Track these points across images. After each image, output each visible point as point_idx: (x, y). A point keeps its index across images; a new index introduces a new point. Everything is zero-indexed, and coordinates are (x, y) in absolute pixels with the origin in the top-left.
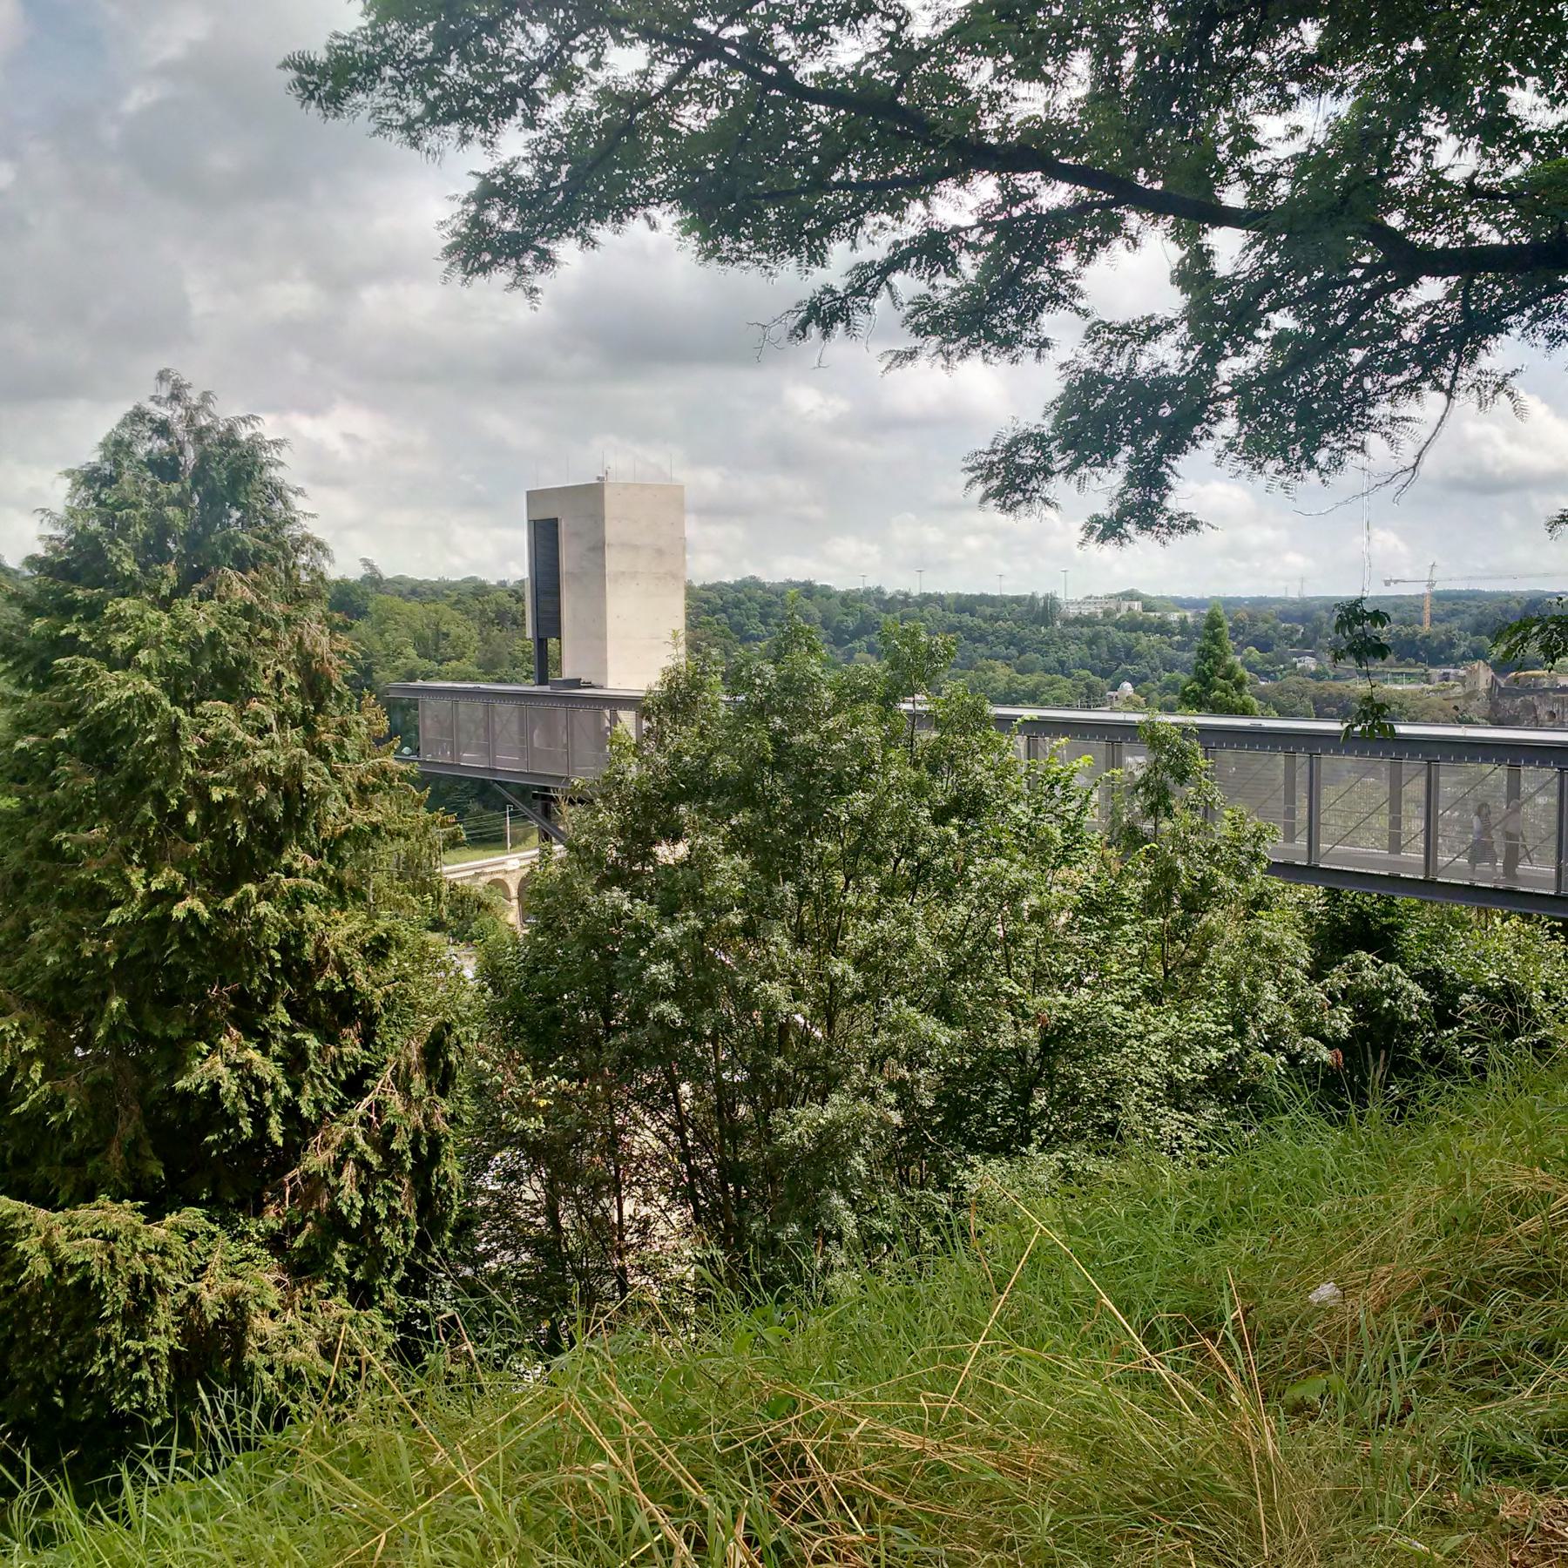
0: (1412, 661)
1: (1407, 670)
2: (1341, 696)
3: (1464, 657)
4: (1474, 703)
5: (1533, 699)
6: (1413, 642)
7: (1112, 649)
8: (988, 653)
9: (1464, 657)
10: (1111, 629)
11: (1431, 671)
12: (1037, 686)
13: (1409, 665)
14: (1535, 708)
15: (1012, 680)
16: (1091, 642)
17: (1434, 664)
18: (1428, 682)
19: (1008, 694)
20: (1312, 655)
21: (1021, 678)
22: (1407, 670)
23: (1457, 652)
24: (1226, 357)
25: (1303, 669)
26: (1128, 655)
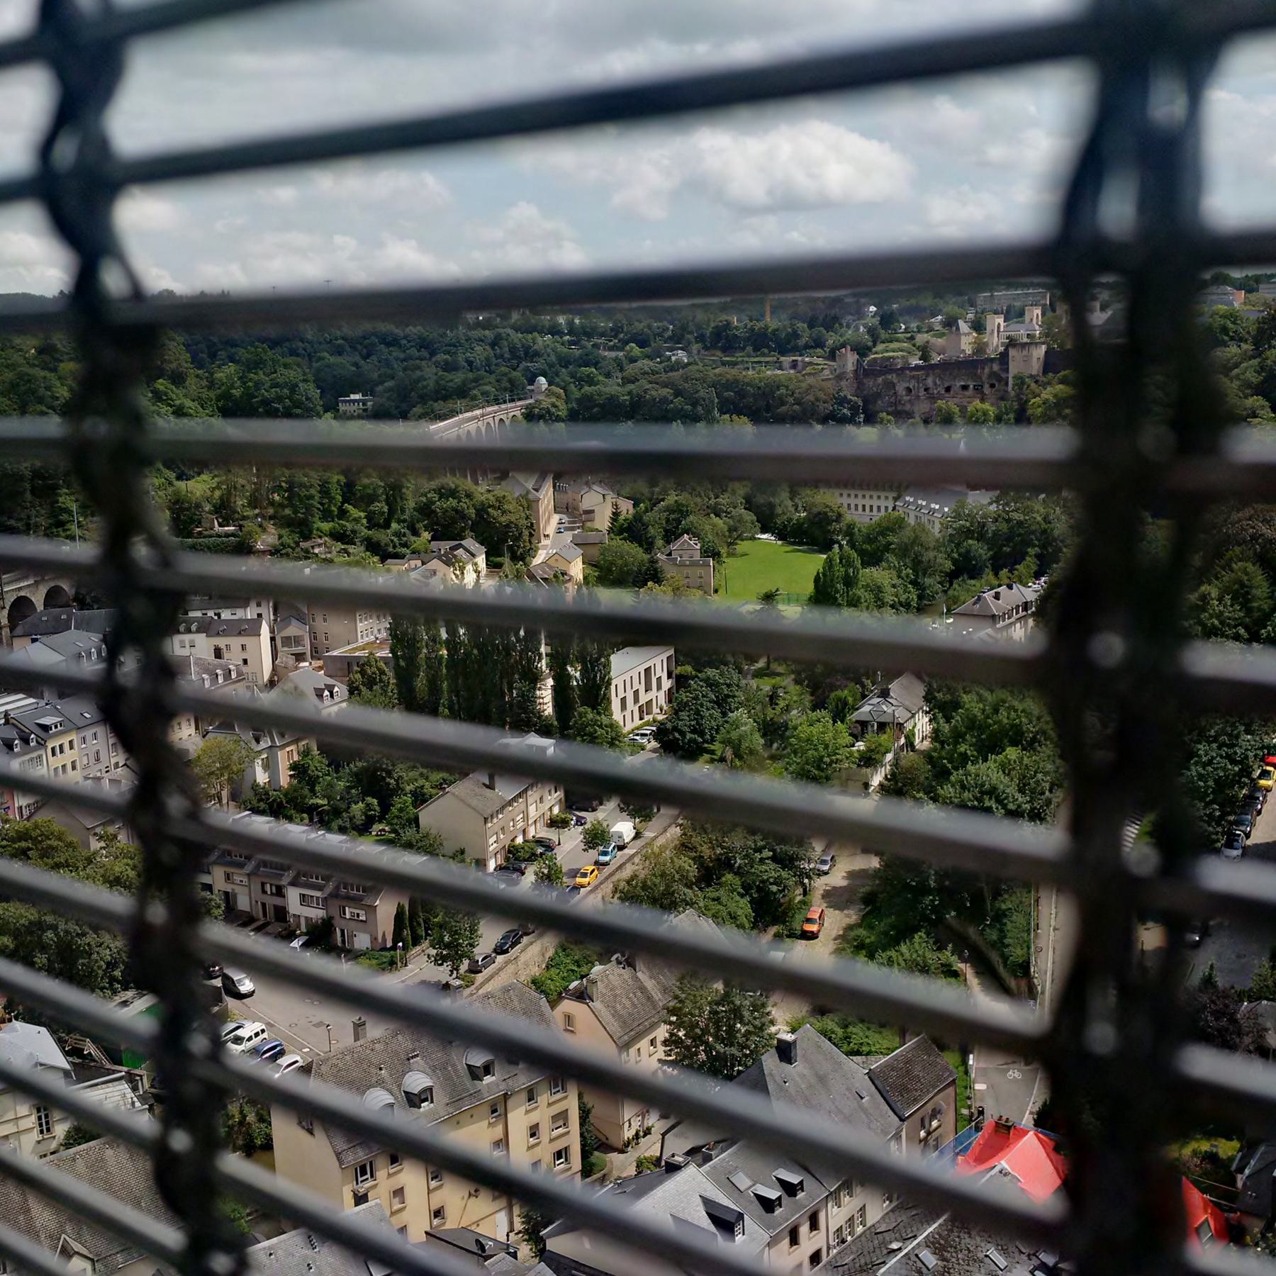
0: (766, 351)
1: (762, 359)
2: (736, 381)
3: (807, 347)
4: (844, 383)
5: (893, 377)
6: (765, 335)
7: (513, 350)
8: (402, 356)
9: (807, 347)
10: (509, 331)
11: (782, 359)
12: (464, 383)
13: (764, 355)
14: (894, 385)
15: (441, 378)
16: (493, 344)
17: (783, 353)
18: (781, 368)
19: (437, 392)
20: (682, 349)
21: (449, 376)
22: (762, 359)
23: (802, 342)
24: (179, 632)
25: (678, 362)
26: (526, 354)
